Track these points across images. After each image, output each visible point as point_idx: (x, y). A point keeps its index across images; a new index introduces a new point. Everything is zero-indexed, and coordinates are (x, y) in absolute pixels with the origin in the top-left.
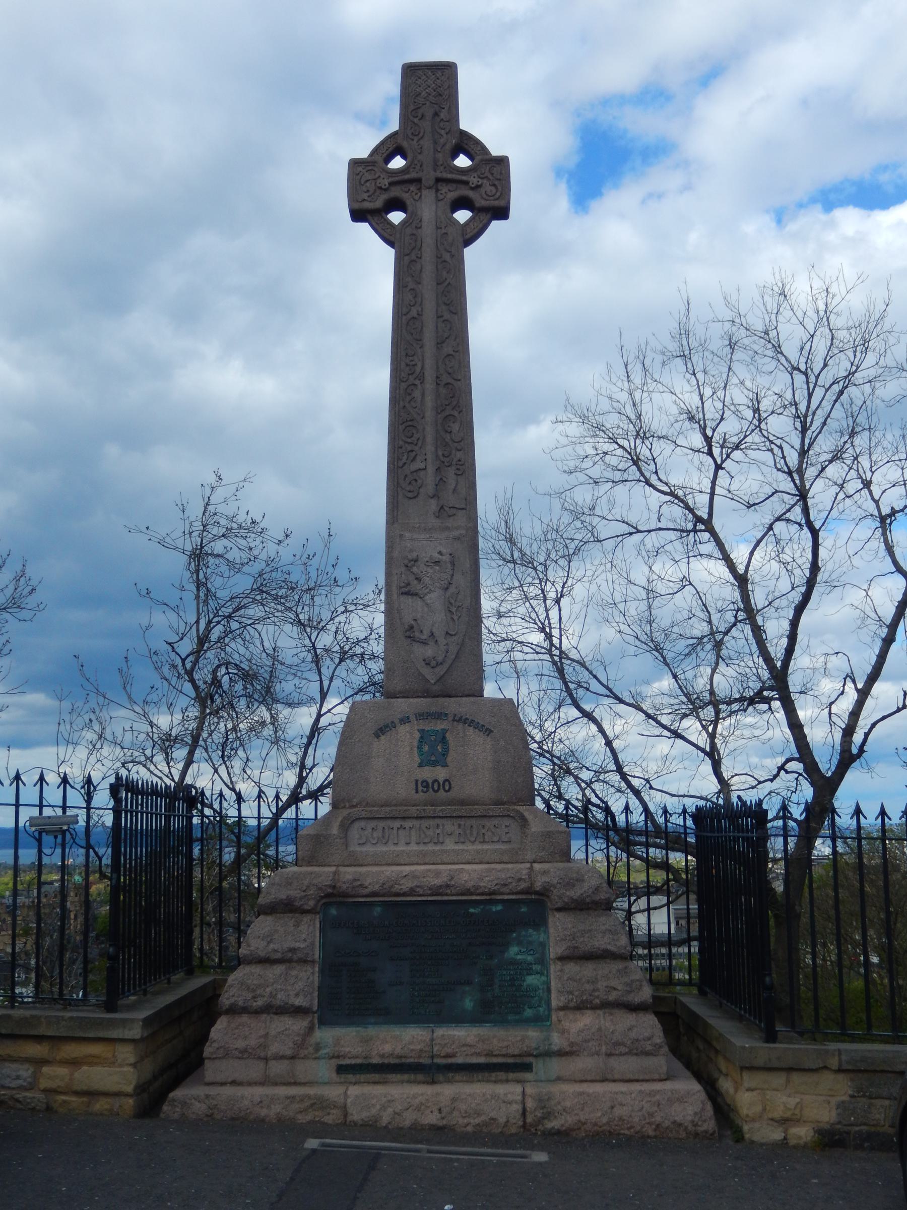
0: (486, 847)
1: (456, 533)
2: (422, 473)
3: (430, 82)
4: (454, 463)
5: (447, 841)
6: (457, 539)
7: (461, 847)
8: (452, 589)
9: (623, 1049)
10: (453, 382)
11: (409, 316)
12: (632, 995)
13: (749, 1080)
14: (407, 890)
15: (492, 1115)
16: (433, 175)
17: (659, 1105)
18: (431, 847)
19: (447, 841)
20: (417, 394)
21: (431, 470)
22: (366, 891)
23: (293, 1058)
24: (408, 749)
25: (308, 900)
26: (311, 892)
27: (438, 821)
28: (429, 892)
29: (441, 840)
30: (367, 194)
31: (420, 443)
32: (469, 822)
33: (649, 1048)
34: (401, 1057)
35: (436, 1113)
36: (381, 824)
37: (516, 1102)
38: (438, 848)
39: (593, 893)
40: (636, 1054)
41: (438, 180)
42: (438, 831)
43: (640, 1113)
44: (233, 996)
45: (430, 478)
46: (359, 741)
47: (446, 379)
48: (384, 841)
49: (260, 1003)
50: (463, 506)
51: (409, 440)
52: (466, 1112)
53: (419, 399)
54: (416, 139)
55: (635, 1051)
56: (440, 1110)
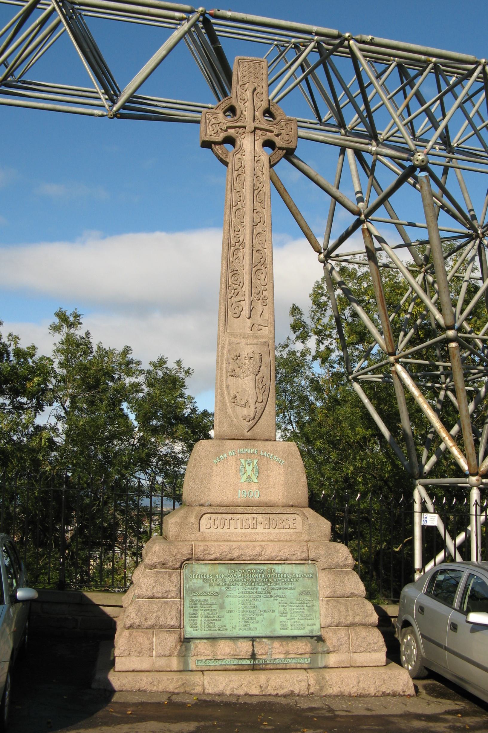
0: (282, 531)
1: (263, 341)
2: (242, 303)
3: (252, 70)
4: (261, 298)
5: (259, 527)
6: (263, 344)
7: (267, 531)
8: (260, 375)
9: (362, 649)
10: (262, 249)
11: (237, 207)
12: (367, 619)
13: (399, 689)
14: (236, 557)
15: (291, 689)
16: (253, 125)
17: (384, 680)
18: (249, 530)
19: (259, 527)
20: (240, 255)
21: (247, 301)
22: (213, 557)
23: (170, 656)
24: (234, 471)
25: (177, 562)
26: (179, 557)
27: (253, 515)
28: (249, 558)
29: (255, 527)
30: (213, 132)
31: (241, 284)
32: (272, 516)
33: (376, 648)
34: (235, 655)
35: (258, 688)
36: (220, 516)
37: (304, 681)
38: (254, 531)
39: (344, 560)
40: (369, 652)
41: (256, 128)
42: (254, 522)
43: (374, 686)
44: (132, 619)
45: (245, 305)
46: (205, 465)
47: (257, 247)
48: (222, 527)
49: (150, 623)
50: (266, 325)
51: (235, 282)
52: (275, 687)
53: (242, 258)
54: (243, 102)
55: (369, 650)
56: (261, 687)
